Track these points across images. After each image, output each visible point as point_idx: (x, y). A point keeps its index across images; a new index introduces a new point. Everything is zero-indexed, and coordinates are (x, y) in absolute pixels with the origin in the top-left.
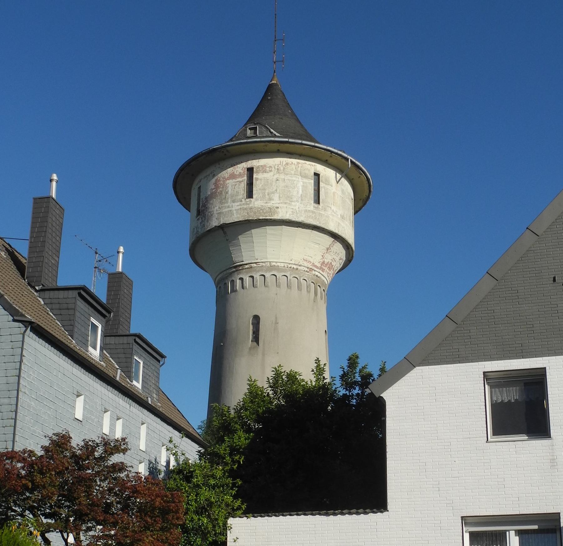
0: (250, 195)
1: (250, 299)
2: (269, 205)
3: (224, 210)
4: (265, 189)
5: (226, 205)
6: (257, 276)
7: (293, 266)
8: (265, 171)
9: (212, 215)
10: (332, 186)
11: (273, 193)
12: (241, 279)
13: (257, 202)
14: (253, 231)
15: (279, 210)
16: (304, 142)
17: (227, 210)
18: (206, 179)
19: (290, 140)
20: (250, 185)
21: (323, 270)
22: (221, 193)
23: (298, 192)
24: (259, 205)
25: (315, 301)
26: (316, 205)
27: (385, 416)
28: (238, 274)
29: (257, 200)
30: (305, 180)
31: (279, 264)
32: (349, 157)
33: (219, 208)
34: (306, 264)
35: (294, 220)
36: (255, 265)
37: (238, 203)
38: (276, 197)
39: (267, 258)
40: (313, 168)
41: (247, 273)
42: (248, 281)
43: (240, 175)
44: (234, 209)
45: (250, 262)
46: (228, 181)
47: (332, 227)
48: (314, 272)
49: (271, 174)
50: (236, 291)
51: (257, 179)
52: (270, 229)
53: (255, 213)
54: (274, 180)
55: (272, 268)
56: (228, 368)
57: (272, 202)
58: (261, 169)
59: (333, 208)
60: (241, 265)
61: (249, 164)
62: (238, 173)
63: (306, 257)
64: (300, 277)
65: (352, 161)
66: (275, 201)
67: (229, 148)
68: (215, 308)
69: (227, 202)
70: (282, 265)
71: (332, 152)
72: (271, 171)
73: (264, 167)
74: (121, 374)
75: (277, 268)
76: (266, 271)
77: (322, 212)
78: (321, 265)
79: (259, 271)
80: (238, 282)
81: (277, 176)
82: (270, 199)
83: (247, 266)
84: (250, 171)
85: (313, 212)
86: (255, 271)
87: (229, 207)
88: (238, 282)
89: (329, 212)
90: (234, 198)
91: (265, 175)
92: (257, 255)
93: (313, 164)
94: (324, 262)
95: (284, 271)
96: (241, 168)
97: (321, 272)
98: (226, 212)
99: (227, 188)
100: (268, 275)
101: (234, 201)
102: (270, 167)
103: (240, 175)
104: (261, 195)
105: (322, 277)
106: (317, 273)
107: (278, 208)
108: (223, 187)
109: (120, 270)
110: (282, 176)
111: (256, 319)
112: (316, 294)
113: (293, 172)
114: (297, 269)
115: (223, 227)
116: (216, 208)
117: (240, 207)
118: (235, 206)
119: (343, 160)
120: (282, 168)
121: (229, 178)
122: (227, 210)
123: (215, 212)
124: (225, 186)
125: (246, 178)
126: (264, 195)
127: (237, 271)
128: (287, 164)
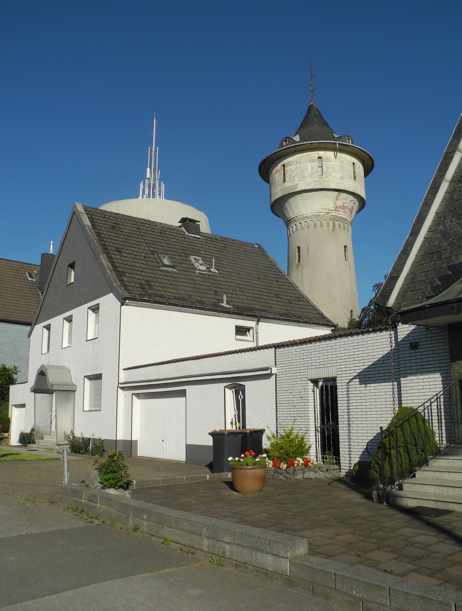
0: (284, 181)
2: (293, 184)
4: (291, 175)
7: (315, 214)
8: (290, 165)
10: (331, 161)
11: (295, 176)
12: (292, 227)
13: (288, 184)
14: (290, 200)
15: (299, 185)
16: (304, 143)
21: (338, 211)
23: (308, 172)
30: (312, 164)
31: (308, 215)
32: (336, 142)
34: (324, 211)
35: (307, 189)
38: (296, 178)
40: (317, 155)
47: (333, 186)
48: (331, 214)
49: (293, 165)
51: (287, 170)
52: (297, 197)
57: (295, 181)
59: (333, 174)
61: (281, 164)
63: (322, 207)
64: (321, 219)
65: (338, 143)
67: (270, 157)
70: (310, 215)
71: (324, 143)
73: (289, 162)
74: (95, 232)
75: (307, 217)
77: (325, 179)
78: (335, 208)
80: (294, 227)
82: (294, 180)
83: (293, 220)
85: (318, 181)
89: (330, 178)
91: (291, 167)
93: (317, 152)
94: (337, 207)
97: (336, 212)
100: (302, 222)
105: (339, 215)
106: (333, 214)
107: (298, 184)
109: (51, 252)
110: (299, 165)
111: (299, 248)
112: (334, 226)
113: (305, 161)
114: (319, 215)
115: (280, 198)
119: (334, 145)
121: (276, 173)
128: (301, 157)
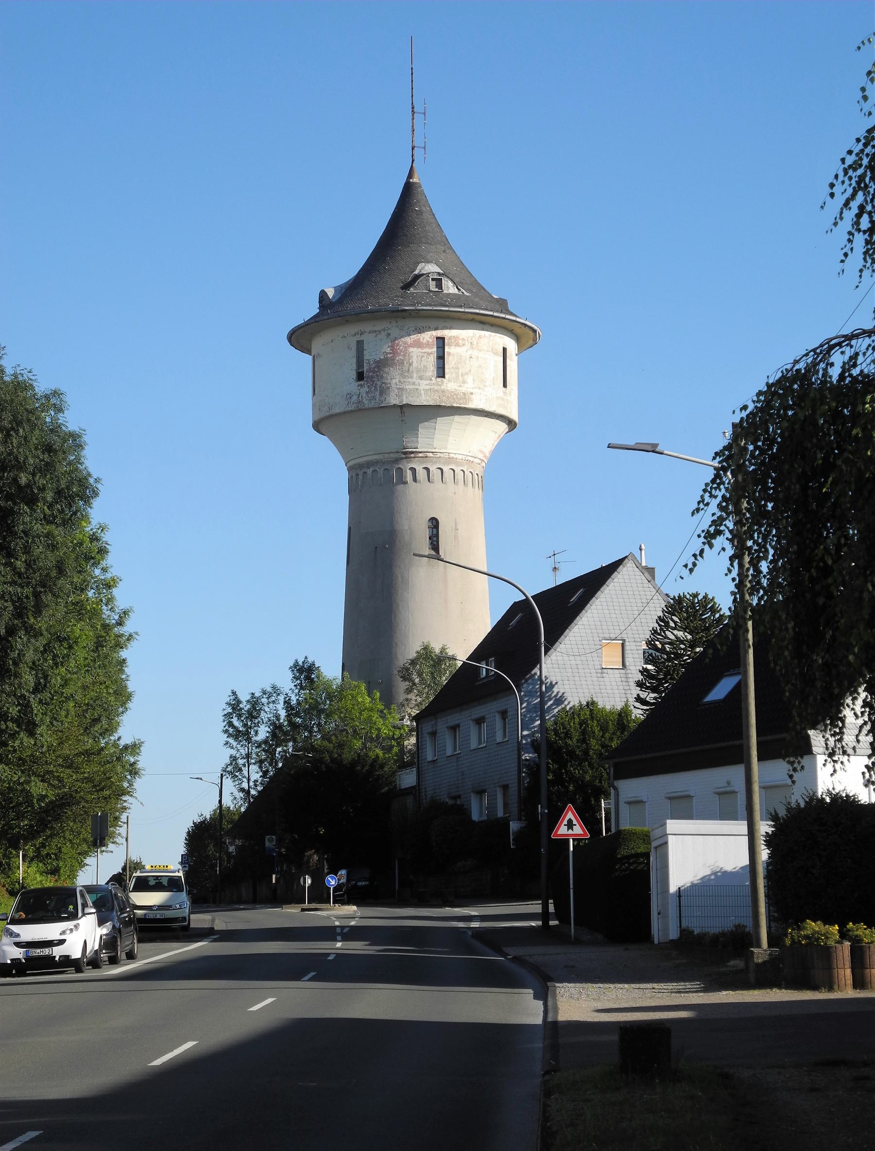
1: (422, 500)
2: (463, 389)
3: (407, 387)
5: (410, 380)
6: (433, 468)
8: (457, 345)
9: (389, 388)
11: (467, 374)
12: (413, 470)
13: (449, 384)
15: (473, 397)
17: (411, 387)
18: (374, 334)
19: (495, 314)
22: (402, 363)
25: (710, 537)
26: (504, 389)
28: (408, 463)
29: (449, 381)
31: (457, 456)
33: (400, 381)
36: (431, 455)
37: (427, 382)
38: (469, 379)
39: (446, 448)
41: (421, 463)
42: (421, 474)
43: (428, 345)
44: (421, 388)
45: (425, 450)
46: (411, 349)
49: (464, 348)
50: (406, 483)
52: (474, 418)
53: (448, 398)
54: (468, 357)
55: (450, 460)
56: (400, 578)
57: (466, 386)
58: (453, 340)
60: (413, 452)
61: (439, 333)
62: (425, 341)
66: (468, 387)
68: (346, 497)
69: (412, 377)
70: (460, 457)
72: (464, 345)
76: (444, 464)
79: (435, 463)
81: (470, 352)
82: (464, 382)
83: (420, 455)
84: (441, 341)
86: (431, 461)
87: (414, 384)
88: (409, 474)
90: (421, 374)
92: (436, 443)
95: (461, 464)
96: (429, 337)
98: (411, 389)
99: (410, 357)
101: (421, 378)
102: (463, 339)
103: (428, 345)
104: (454, 375)
107: (472, 394)
108: (404, 355)
110: (475, 353)
111: (434, 524)
115: (403, 408)
116: (394, 381)
117: (429, 387)
118: (423, 385)
120: (475, 343)
122: (411, 387)
123: (393, 386)
125: (435, 349)
126: (458, 377)
127: (406, 458)
128: (480, 337)
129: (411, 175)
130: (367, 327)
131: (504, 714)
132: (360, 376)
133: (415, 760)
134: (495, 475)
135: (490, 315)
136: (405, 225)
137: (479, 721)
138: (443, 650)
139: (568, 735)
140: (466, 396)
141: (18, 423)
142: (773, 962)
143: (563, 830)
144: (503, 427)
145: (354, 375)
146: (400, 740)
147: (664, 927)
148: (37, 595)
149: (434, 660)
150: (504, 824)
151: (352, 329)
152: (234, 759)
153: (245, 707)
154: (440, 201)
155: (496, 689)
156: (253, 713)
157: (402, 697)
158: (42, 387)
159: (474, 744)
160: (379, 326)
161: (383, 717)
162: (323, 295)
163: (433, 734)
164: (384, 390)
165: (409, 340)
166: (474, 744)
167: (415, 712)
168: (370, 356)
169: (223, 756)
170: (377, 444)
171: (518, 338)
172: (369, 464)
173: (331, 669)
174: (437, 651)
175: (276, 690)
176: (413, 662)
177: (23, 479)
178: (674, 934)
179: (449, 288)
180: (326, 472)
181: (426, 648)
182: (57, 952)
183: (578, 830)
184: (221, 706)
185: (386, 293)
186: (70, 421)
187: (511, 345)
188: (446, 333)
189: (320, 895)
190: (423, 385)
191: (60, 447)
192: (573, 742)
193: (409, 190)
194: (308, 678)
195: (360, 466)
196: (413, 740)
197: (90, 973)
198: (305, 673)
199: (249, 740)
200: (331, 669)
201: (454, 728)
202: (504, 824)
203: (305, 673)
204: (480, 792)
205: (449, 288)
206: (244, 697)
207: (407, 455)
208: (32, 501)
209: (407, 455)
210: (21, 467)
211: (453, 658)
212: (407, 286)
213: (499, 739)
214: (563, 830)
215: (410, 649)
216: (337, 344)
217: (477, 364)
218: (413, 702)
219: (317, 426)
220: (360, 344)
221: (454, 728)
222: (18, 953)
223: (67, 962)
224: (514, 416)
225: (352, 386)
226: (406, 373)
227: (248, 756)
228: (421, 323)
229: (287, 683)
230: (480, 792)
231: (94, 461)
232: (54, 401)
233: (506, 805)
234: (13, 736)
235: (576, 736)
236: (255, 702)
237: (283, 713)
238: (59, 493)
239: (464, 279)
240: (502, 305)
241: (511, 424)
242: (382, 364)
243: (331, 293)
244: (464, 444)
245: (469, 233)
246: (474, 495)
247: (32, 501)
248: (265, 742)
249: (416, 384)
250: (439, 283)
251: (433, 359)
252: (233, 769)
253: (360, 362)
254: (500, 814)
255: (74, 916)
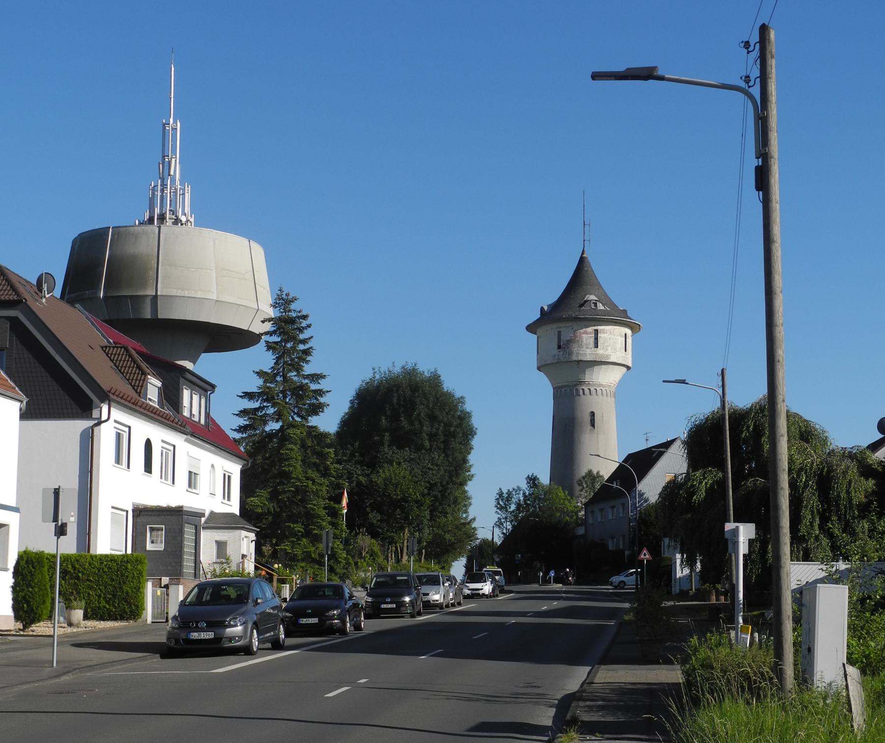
0: (596, 346)
1: (589, 403)
6: (592, 389)
13: (600, 351)
20: (596, 339)
24: (601, 352)
27: (79, 476)
38: (609, 348)
42: (587, 391)
43: (590, 333)
55: (600, 385)
61: (596, 328)
66: (609, 352)
84: (596, 332)
96: (591, 329)
103: (590, 333)
110: (612, 336)
111: (593, 414)
115: (579, 362)
118: (588, 351)
124: (581, 338)
129: (583, 253)
130: (562, 325)
131: (623, 505)
132: (559, 347)
133: (584, 522)
134: (621, 391)
135: (619, 318)
136: (580, 277)
137: (613, 507)
138: (598, 473)
139: (650, 515)
140: (608, 356)
141: (450, 410)
142: (695, 594)
143: (642, 556)
144: (625, 369)
145: (556, 347)
146: (577, 513)
147: (676, 589)
148: (456, 470)
149: (591, 477)
150: (623, 551)
151: (554, 326)
152: (500, 519)
153: (505, 495)
154: (597, 266)
155: (619, 494)
156: (509, 498)
157: (577, 493)
158: (458, 395)
159: (610, 517)
160: (568, 324)
161: (570, 502)
162: (542, 309)
163: (592, 512)
164: (570, 354)
165: (582, 331)
166: (610, 517)
167: (583, 500)
168: (564, 338)
169: (495, 518)
170: (567, 378)
171: (631, 328)
172: (563, 387)
173: (545, 479)
174: (595, 473)
175: (519, 489)
176: (584, 478)
177: (452, 429)
178: (678, 591)
179: (600, 307)
180: (542, 392)
181: (590, 472)
182: (481, 592)
183: (647, 556)
184: (494, 495)
185: (570, 311)
186: (468, 407)
187: (629, 332)
188: (599, 328)
189: (546, 581)
190: (588, 351)
191: (465, 417)
192: (652, 519)
193: (582, 261)
194: (534, 483)
195: (559, 387)
196: (583, 513)
197: (446, 610)
198: (533, 481)
199: (507, 511)
200: (545, 479)
201: (602, 510)
202: (623, 551)
203: (533, 481)
204: (613, 538)
205: (600, 307)
206: (505, 491)
207: (581, 383)
208: (454, 437)
209: (581, 383)
210: (451, 426)
211: (602, 477)
212: (582, 305)
213: (621, 515)
214: (642, 556)
215: (583, 472)
216: (550, 331)
217: (613, 341)
218: (582, 498)
219: (539, 368)
220: (559, 332)
221: (602, 510)
222: (469, 592)
223: (483, 594)
224: (630, 364)
225: (556, 351)
226: (580, 346)
227: (506, 518)
228: (587, 323)
229: (524, 485)
230: (613, 538)
231: (475, 422)
232: (461, 400)
233: (624, 544)
234: (439, 517)
235: (653, 515)
236: (509, 493)
237: (522, 499)
238: (464, 433)
239: (607, 301)
240: (625, 312)
241: (628, 368)
242: (569, 342)
243: (546, 308)
244: (607, 378)
245: (612, 282)
246: (611, 401)
247: (454, 437)
248: (513, 511)
249: (587, 353)
250: (596, 305)
251: (592, 339)
252: (499, 524)
253: (559, 341)
254: (621, 547)
255: (485, 581)
